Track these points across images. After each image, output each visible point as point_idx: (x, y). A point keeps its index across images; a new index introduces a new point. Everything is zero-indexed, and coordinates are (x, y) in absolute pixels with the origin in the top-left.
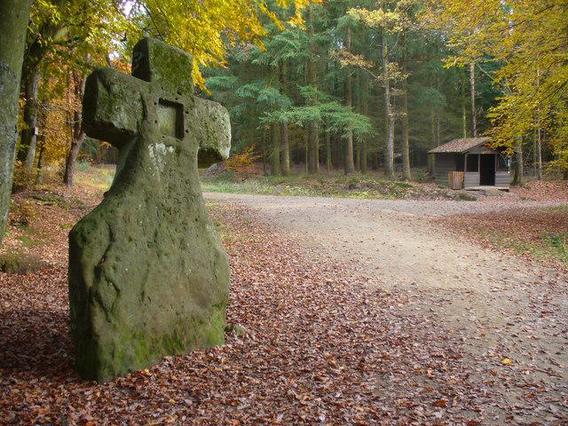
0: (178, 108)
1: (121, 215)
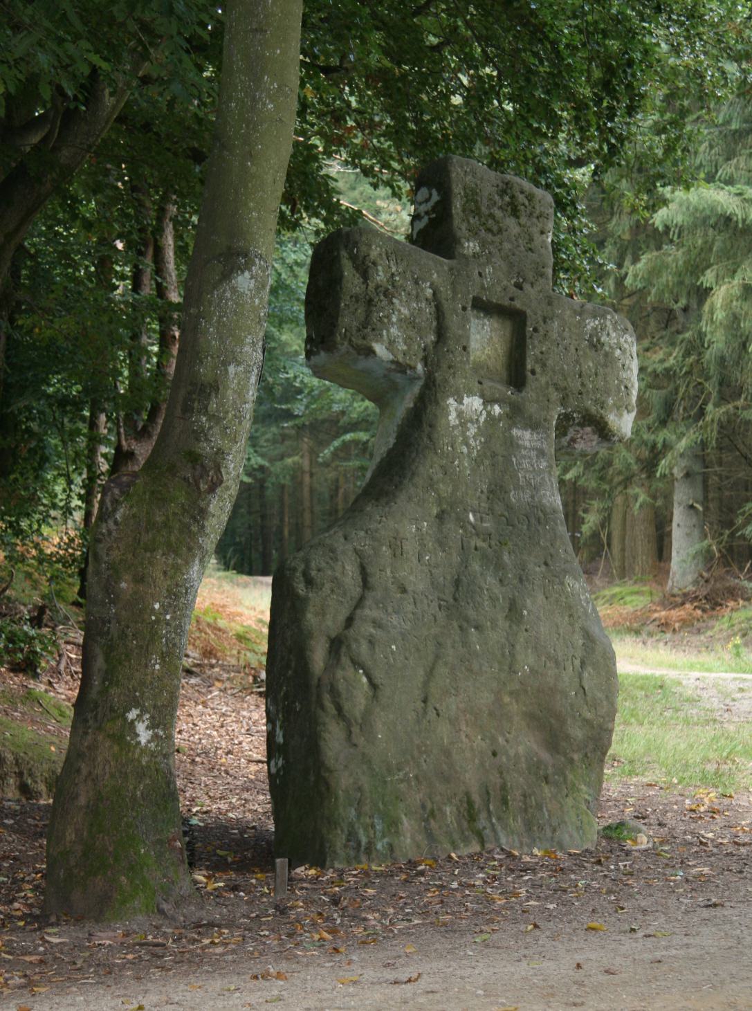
0: (514, 319)
1: (82, 801)
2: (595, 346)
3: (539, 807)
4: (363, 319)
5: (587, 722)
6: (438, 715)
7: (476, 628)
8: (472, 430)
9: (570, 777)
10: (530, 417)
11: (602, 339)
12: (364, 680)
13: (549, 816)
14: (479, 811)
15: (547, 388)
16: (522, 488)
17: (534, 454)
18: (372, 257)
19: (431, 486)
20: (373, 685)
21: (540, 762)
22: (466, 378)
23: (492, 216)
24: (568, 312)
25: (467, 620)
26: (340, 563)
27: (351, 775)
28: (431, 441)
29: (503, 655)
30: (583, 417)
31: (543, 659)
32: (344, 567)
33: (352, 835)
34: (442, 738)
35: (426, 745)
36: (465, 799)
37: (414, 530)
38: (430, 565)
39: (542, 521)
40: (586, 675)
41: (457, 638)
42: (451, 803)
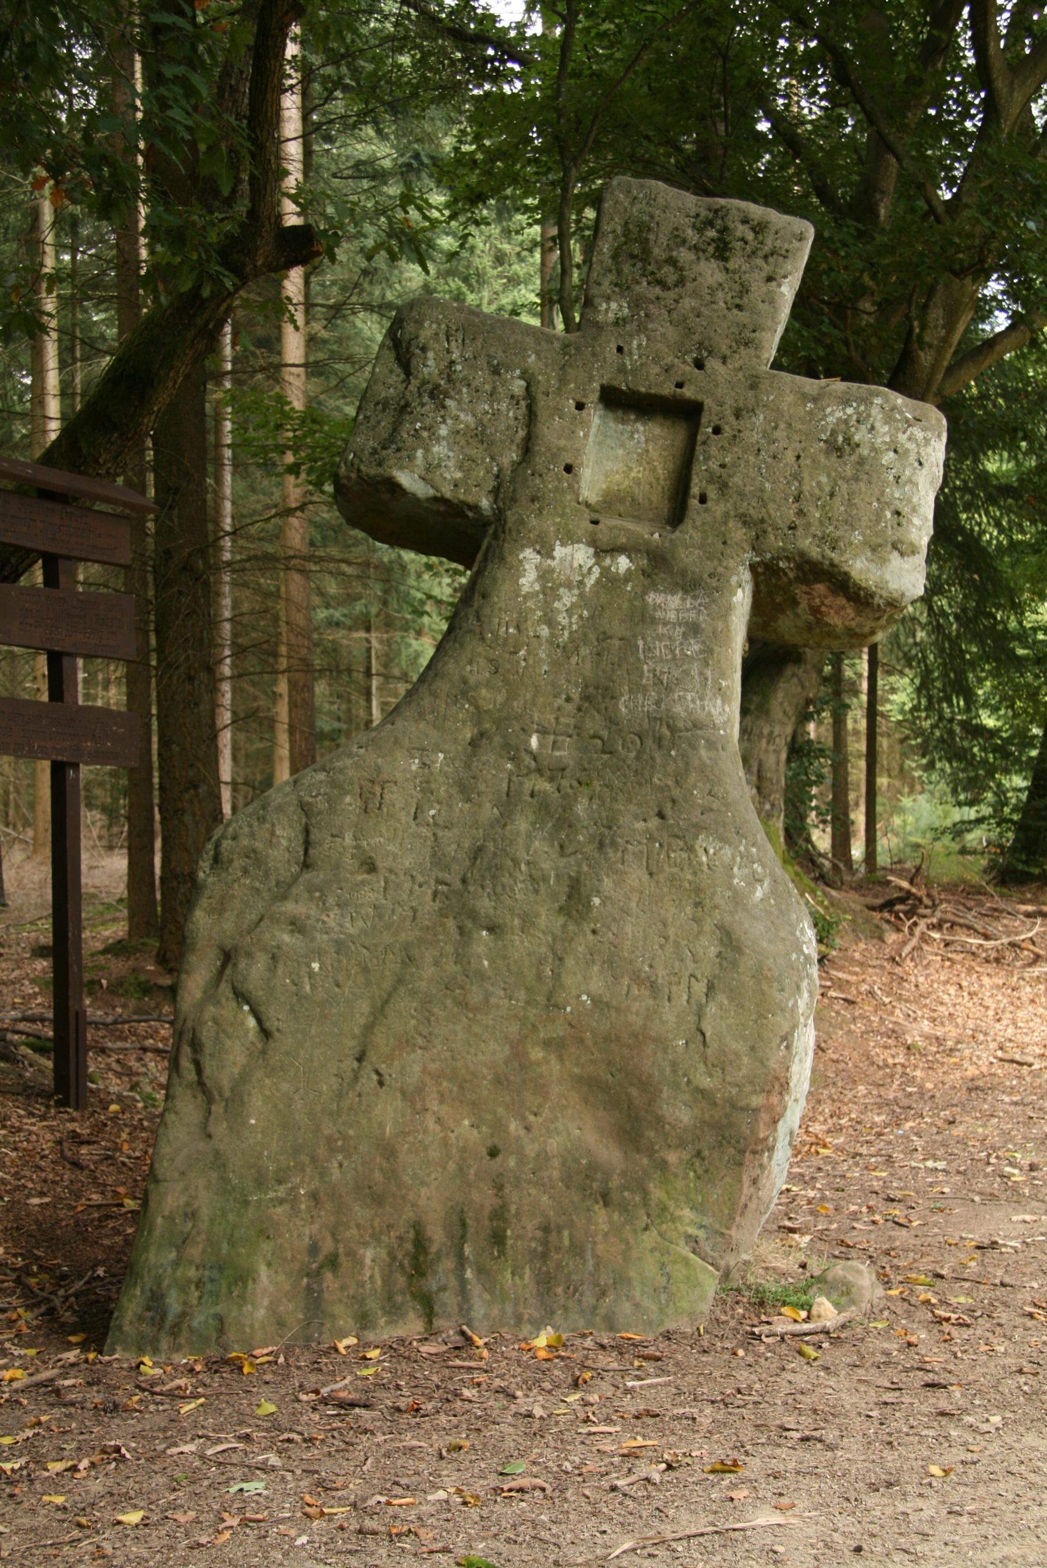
2: (839, 449)
3: (577, 1250)
4: (386, 436)
5: (703, 1093)
6: (381, 1083)
7: (491, 929)
8: (568, 598)
9: (657, 1193)
10: (683, 573)
11: (857, 438)
12: (252, 1022)
13: (597, 1265)
14: (439, 1255)
15: (725, 523)
16: (645, 689)
17: (679, 631)
18: (422, 340)
19: (464, 693)
20: (265, 1033)
21: (593, 1167)
22: (562, 516)
23: (672, 262)
24: (790, 398)
25: (473, 915)
26: (268, 826)
27: (186, 1189)
28: (479, 620)
29: (539, 977)
30: (799, 567)
31: (626, 981)
32: (273, 833)
33: (156, 1301)
34: (381, 1126)
35: (345, 1138)
36: (412, 1235)
37: (414, 768)
38: (436, 824)
39: (665, 743)
40: (712, 1009)
41: (449, 948)
42: (379, 1241)
